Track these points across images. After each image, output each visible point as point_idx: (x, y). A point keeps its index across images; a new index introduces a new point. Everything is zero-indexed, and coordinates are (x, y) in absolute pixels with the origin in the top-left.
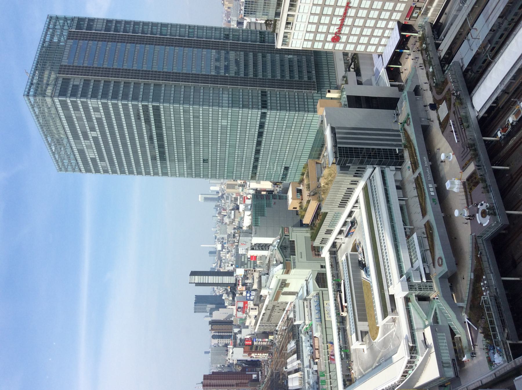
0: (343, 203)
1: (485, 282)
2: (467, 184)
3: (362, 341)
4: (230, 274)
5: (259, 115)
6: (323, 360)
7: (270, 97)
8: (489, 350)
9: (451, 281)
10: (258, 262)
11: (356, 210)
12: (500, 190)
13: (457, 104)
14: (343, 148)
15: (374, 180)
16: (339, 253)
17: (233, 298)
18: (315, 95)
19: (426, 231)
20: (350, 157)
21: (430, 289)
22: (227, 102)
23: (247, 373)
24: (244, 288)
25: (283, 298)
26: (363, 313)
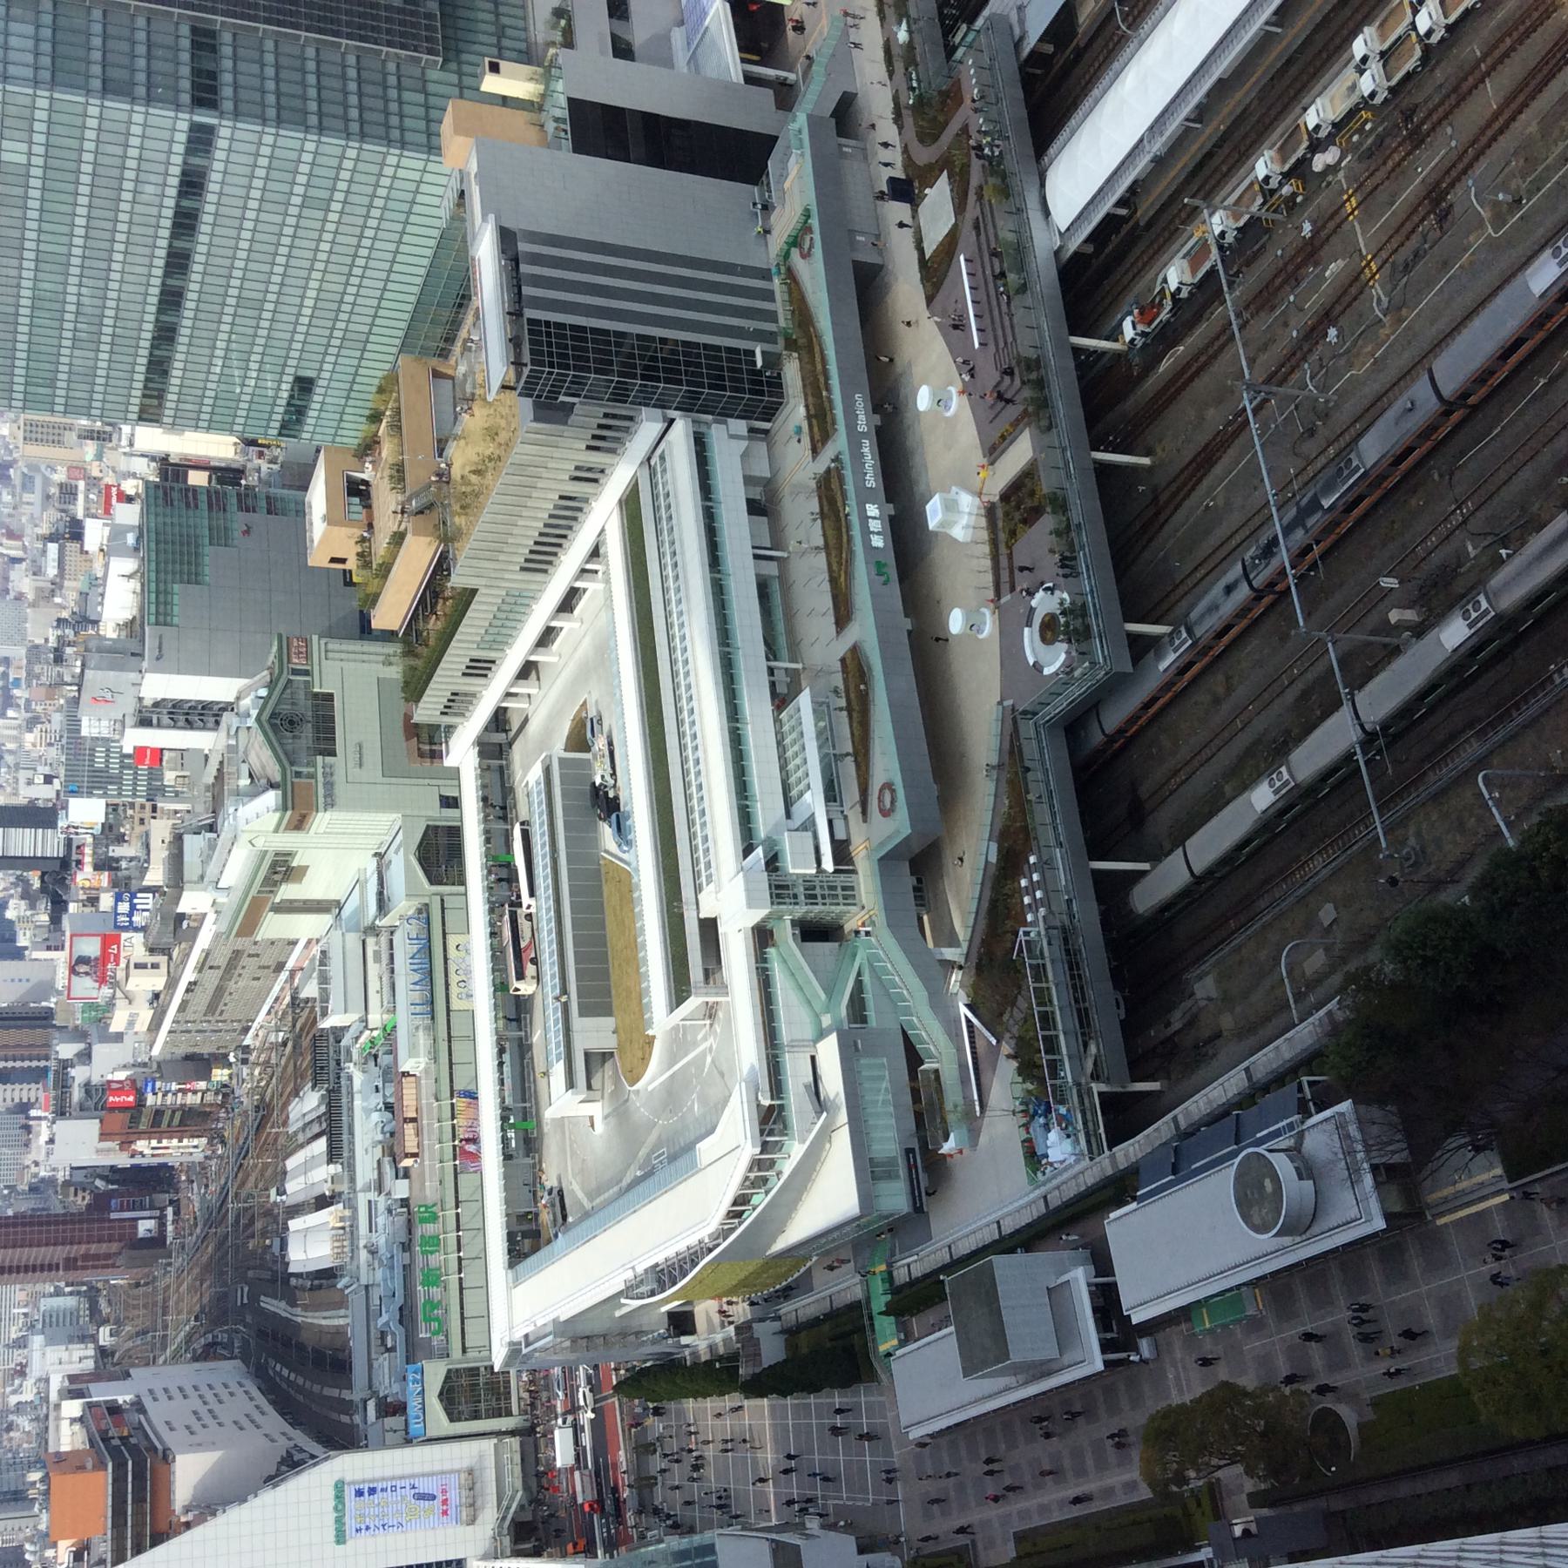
0: (542, 556)
1: (1035, 877)
2: (1000, 513)
3: (589, 1087)
4: (39, 816)
5: (182, 137)
6: (432, 1165)
7: (235, 58)
8: (1033, 1117)
9: (919, 867)
10: (169, 777)
11: (592, 587)
12: (1112, 543)
13: (987, 193)
14: (548, 324)
15: (664, 471)
16: (517, 753)
17: (56, 920)
18: (434, 74)
19: (845, 680)
20: (576, 368)
21: (845, 897)
22: (30, 44)
23: (113, 1216)
24: (104, 879)
25: (274, 926)
26: (600, 982)
